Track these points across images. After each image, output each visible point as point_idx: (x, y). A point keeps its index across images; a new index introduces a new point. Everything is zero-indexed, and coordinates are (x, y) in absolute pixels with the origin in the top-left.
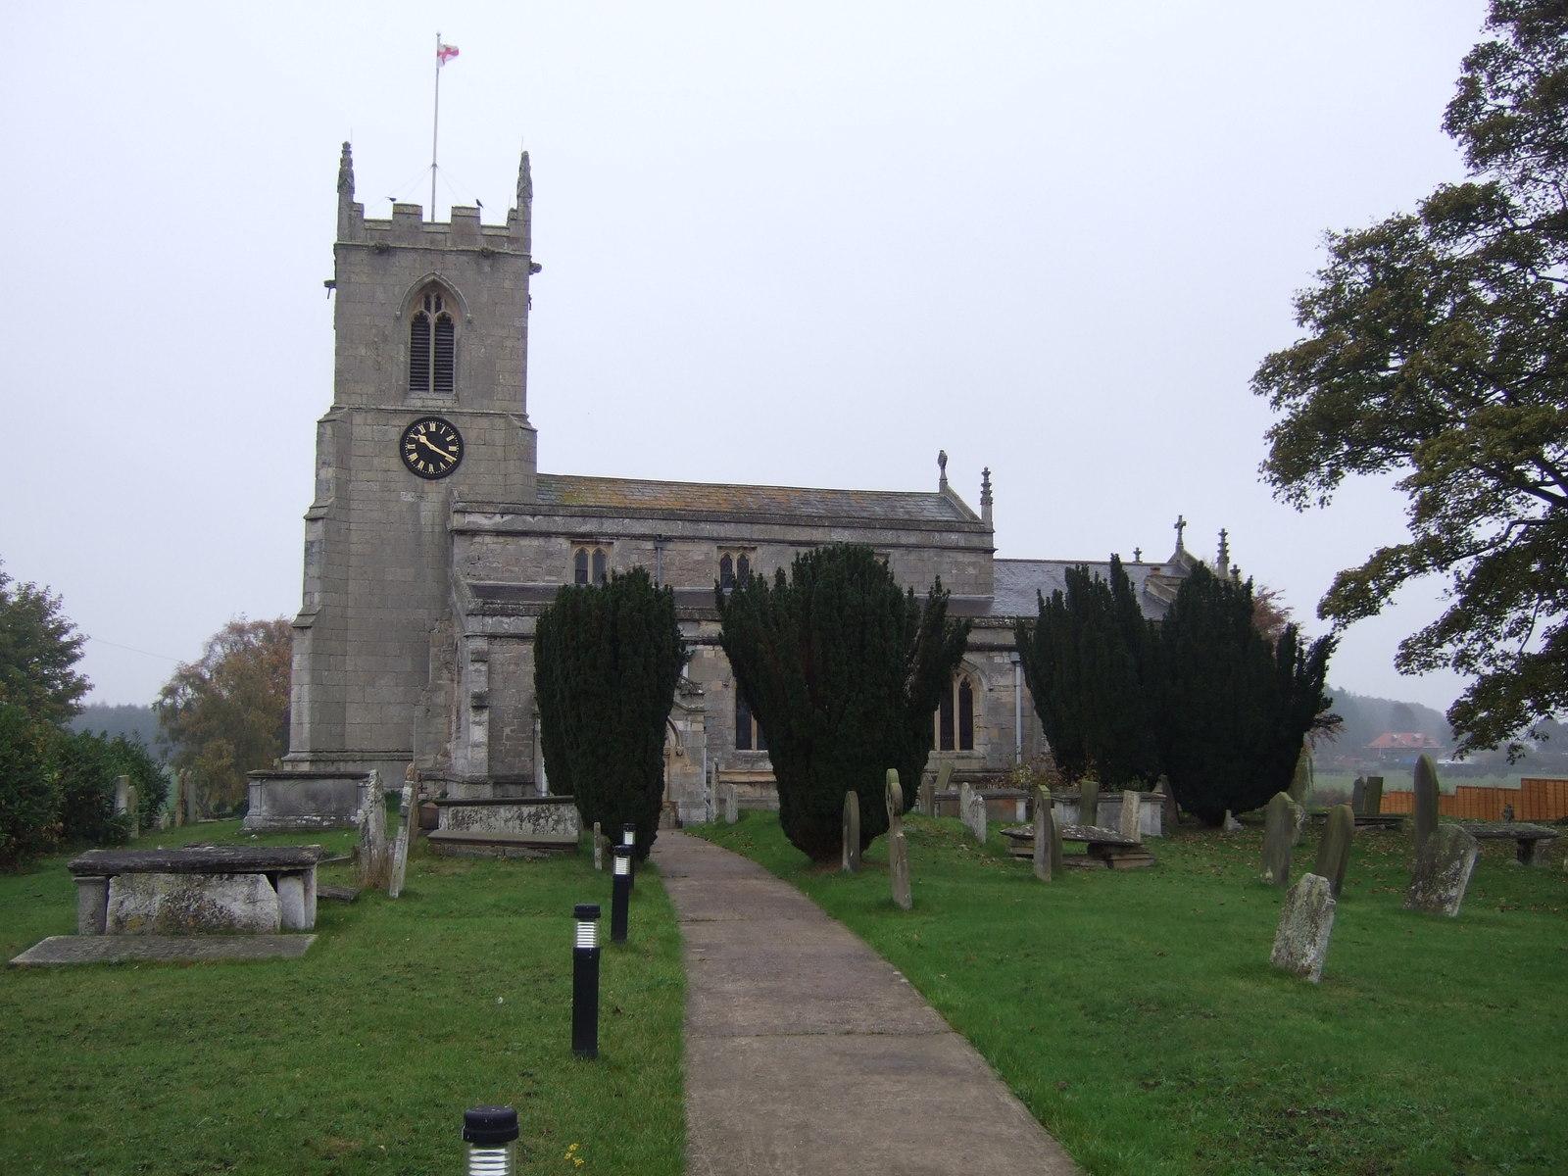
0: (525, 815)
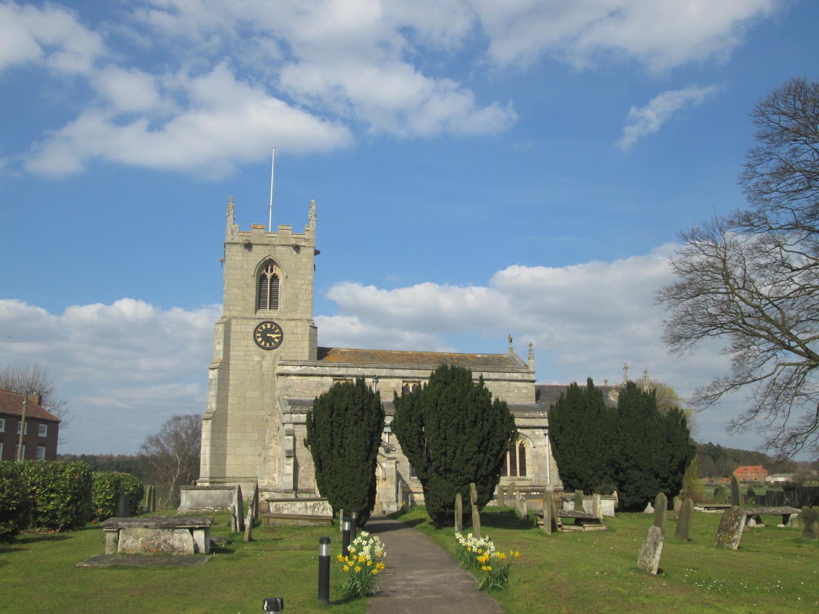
0: (308, 506)
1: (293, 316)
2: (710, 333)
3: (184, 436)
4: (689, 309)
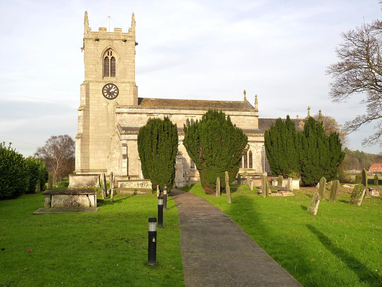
0: (139, 184)
1: (124, 80)
2: (357, 90)
3: (59, 147)
4: (346, 77)
